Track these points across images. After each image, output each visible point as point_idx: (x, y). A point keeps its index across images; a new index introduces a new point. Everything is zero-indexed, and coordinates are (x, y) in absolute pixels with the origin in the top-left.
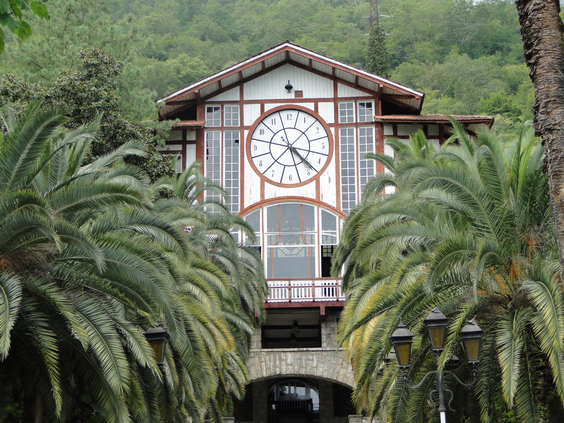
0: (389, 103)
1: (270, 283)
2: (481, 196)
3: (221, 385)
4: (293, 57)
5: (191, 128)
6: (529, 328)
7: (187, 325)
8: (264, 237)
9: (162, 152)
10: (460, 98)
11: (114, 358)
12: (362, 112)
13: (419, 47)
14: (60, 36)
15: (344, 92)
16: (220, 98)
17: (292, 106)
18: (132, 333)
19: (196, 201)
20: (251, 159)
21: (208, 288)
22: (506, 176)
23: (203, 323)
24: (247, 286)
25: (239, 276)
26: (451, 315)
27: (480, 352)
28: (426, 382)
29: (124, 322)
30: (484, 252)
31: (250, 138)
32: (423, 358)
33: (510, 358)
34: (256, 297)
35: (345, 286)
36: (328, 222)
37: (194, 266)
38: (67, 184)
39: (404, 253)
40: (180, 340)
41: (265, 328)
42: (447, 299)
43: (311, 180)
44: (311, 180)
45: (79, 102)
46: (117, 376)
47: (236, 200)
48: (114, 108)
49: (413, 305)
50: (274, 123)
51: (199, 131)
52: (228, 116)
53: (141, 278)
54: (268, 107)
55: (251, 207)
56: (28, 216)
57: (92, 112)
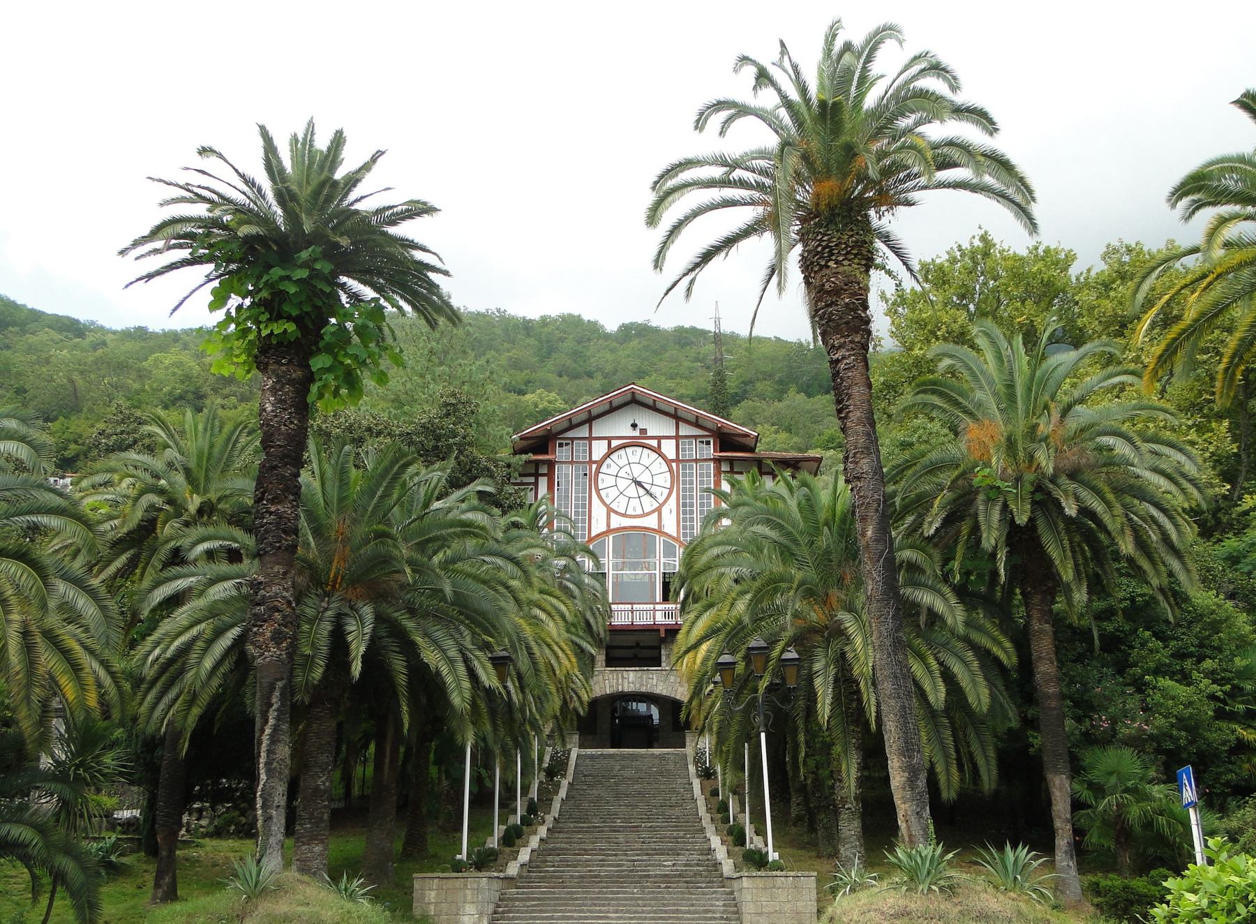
0: (726, 441)
1: (614, 607)
2: (801, 533)
3: (565, 703)
4: (638, 397)
5: (544, 462)
6: (843, 654)
7: (529, 648)
8: (609, 562)
9: (515, 484)
10: (797, 434)
11: (458, 680)
12: (701, 449)
13: (760, 386)
14: (422, 376)
15: (685, 430)
16: (570, 434)
17: (639, 441)
18: (477, 657)
19: (546, 530)
20: (598, 491)
21: (553, 613)
22: (823, 515)
23: (549, 646)
24: (591, 609)
25: (584, 601)
26: (772, 643)
27: (798, 675)
28: (748, 704)
29: (471, 647)
30: (799, 586)
31: (598, 472)
32: (746, 680)
33: (825, 683)
34: (600, 620)
35: (683, 610)
36: (669, 551)
37: (541, 592)
38: (421, 518)
39: (736, 581)
40: (523, 663)
41: (609, 648)
42: (768, 626)
43: (653, 511)
44: (653, 511)
45: (438, 438)
46: (460, 696)
47: (583, 529)
48: (471, 444)
49: (738, 633)
50: (620, 458)
51: (551, 464)
52: (578, 451)
53: (486, 606)
54: (615, 443)
55: (598, 536)
56: (382, 550)
57: (450, 447)
